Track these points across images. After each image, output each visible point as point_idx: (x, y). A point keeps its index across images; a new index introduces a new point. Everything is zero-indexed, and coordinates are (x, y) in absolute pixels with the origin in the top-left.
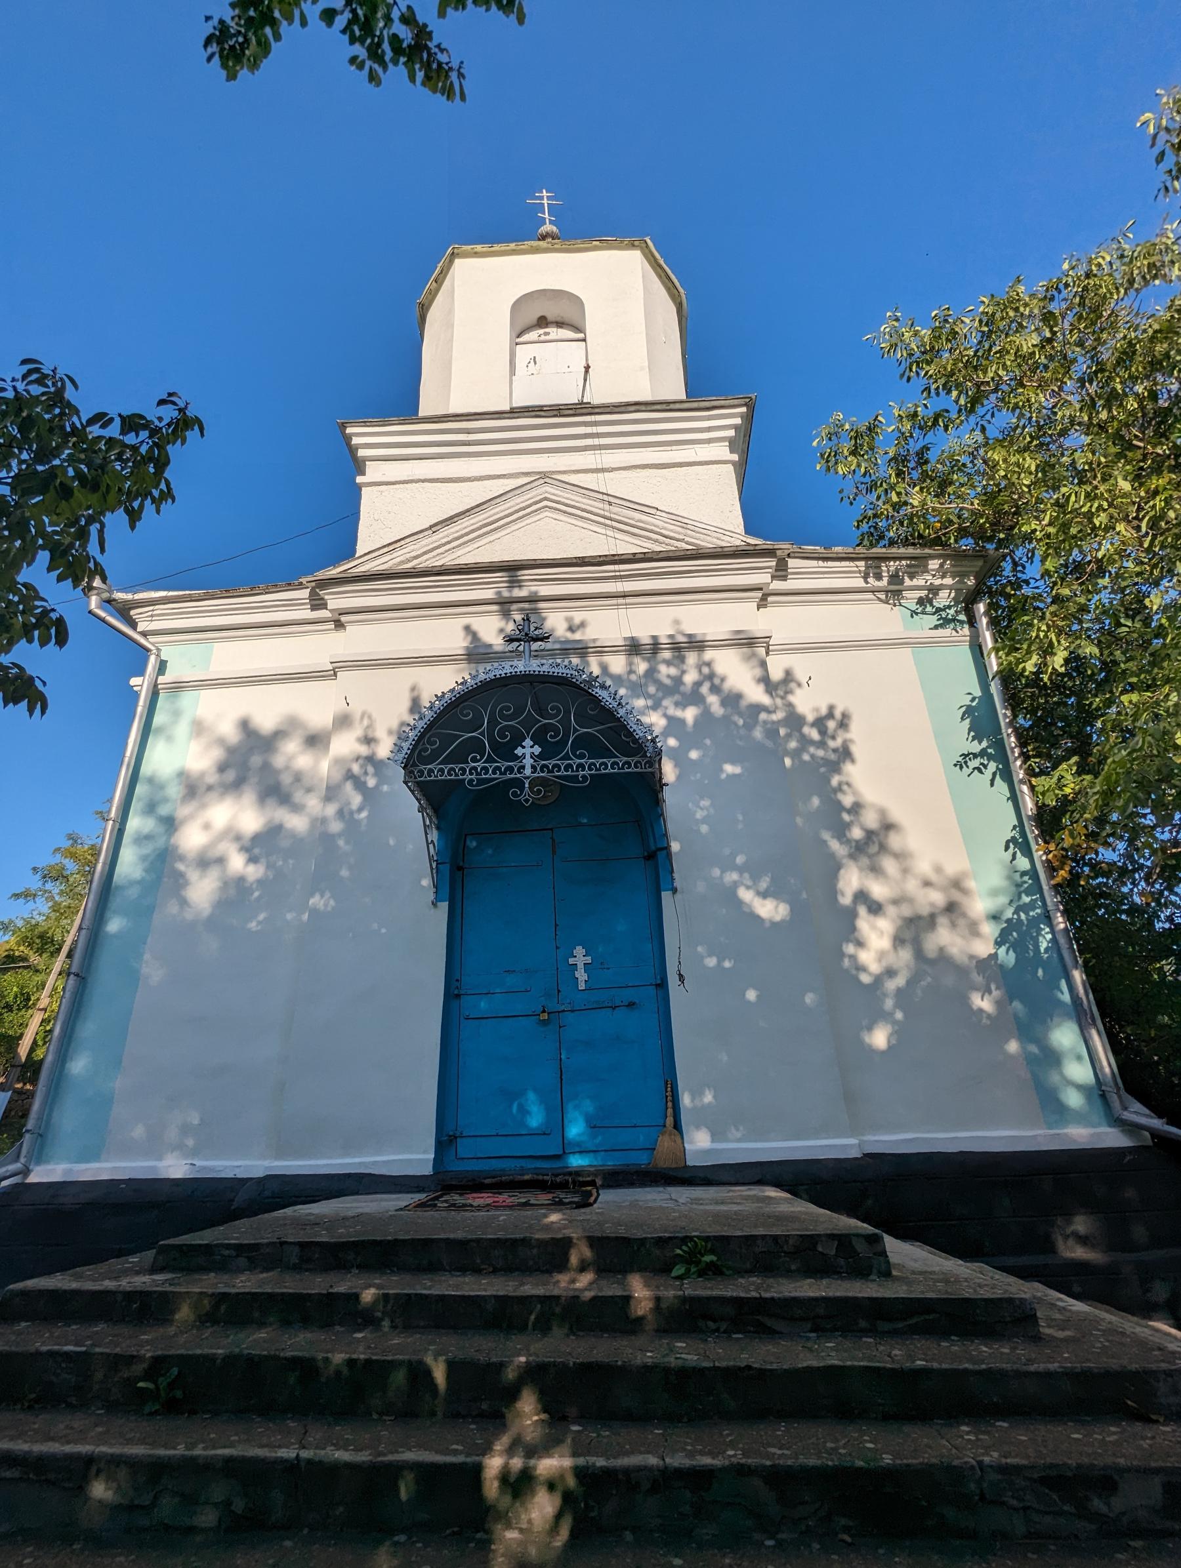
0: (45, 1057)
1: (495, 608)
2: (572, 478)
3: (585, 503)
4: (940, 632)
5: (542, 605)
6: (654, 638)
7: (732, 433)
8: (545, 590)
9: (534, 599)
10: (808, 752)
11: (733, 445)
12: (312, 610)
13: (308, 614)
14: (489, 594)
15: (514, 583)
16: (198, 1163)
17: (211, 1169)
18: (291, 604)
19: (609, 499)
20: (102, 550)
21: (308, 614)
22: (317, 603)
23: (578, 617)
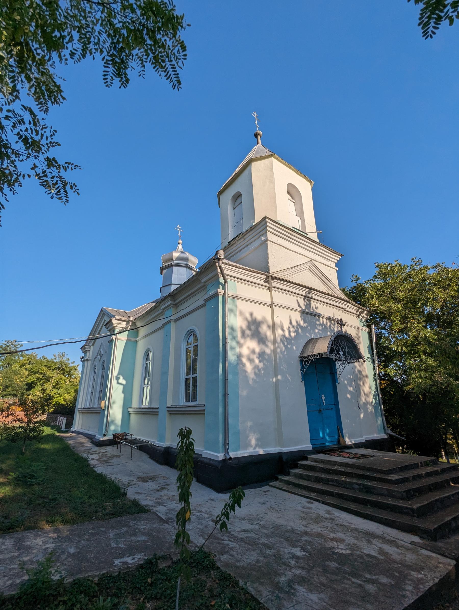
0: (75, 399)
1: (303, 297)
2: (316, 263)
3: (317, 272)
4: (363, 328)
5: (312, 300)
6: (329, 316)
7: (337, 262)
8: (314, 297)
9: (311, 298)
10: (317, 328)
11: (337, 265)
12: (264, 282)
13: (262, 283)
14: (304, 294)
15: (309, 293)
16: (265, 449)
17: (267, 451)
18: (260, 278)
19: (323, 274)
20: (297, 300)
21: (262, 283)
22: (266, 281)
23: (317, 305)
